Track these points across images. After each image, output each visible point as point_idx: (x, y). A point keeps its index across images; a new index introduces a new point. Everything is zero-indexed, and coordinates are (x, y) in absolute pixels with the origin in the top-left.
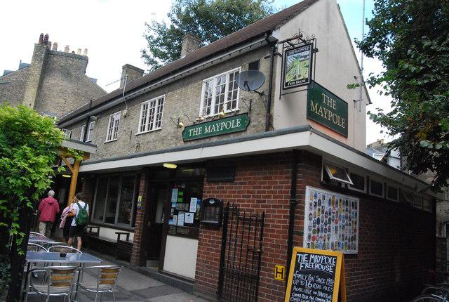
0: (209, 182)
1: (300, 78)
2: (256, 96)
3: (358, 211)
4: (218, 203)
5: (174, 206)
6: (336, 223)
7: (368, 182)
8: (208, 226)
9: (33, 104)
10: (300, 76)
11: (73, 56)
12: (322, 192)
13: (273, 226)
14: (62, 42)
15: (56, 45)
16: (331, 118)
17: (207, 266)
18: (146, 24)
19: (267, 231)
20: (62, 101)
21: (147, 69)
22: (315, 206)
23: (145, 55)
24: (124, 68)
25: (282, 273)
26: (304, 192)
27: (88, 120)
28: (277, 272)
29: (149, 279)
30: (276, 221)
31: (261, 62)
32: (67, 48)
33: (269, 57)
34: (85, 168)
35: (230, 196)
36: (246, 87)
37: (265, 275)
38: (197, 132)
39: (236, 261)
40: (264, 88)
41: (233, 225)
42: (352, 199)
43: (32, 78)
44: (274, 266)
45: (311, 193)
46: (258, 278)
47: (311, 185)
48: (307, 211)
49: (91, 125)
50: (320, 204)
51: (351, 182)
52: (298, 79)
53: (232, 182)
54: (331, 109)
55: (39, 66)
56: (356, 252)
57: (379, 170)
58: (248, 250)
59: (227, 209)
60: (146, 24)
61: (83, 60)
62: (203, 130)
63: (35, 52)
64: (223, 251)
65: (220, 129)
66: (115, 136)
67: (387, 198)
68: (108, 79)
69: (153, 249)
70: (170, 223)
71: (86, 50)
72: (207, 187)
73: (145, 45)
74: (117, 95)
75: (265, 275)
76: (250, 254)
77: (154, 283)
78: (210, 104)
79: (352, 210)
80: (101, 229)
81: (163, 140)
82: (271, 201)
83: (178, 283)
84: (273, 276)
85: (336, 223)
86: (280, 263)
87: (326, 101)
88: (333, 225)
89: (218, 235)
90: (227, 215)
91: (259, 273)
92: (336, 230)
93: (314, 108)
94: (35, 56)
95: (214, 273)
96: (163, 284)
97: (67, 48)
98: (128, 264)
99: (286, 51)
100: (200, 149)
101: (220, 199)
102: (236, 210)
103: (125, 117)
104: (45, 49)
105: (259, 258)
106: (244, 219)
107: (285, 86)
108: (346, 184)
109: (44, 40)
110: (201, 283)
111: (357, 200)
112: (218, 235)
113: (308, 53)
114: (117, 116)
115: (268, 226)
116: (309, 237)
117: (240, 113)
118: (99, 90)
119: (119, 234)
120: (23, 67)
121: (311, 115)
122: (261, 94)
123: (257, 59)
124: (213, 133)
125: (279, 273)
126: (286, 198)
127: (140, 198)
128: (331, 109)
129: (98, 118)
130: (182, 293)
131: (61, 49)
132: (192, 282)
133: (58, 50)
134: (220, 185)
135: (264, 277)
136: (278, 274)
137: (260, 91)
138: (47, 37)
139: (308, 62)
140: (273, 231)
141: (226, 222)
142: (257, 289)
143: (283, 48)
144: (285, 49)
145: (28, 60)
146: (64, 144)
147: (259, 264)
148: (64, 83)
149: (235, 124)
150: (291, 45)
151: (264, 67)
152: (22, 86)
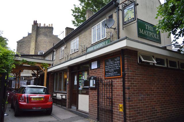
1: (130, 19)
2: (113, 30)
7: (179, 64)
10: (130, 18)
11: (47, 28)
13: (117, 86)
14: (43, 22)
15: (40, 24)
16: (151, 35)
17: (93, 107)
18: (72, 10)
19: (114, 88)
20: (45, 46)
21: (75, 28)
23: (74, 22)
24: (66, 29)
25: (122, 108)
27: (54, 51)
28: (120, 108)
29: (71, 113)
32: (45, 25)
33: (116, 12)
34: (49, 70)
35: (99, 75)
36: (106, 26)
37: (115, 109)
39: (104, 104)
40: (115, 26)
43: (32, 38)
44: (118, 105)
46: (112, 111)
49: (55, 53)
51: (155, 62)
52: (130, 19)
54: (151, 31)
55: (35, 33)
57: (177, 56)
58: (107, 98)
60: (72, 10)
63: (32, 28)
64: (98, 100)
66: (63, 56)
67: (169, 67)
68: (60, 33)
69: (74, 101)
70: (79, 89)
71: (52, 24)
73: (73, 19)
74: (65, 39)
75: (115, 109)
77: (75, 115)
80: (57, 94)
83: (82, 115)
84: (118, 110)
86: (121, 103)
89: (95, 92)
90: (98, 83)
91: (112, 109)
93: (141, 31)
94: (33, 30)
95: (96, 110)
96: (77, 116)
97: (45, 25)
98: (65, 107)
99: (123, 8)
100: (85, 56)
101: (95, 76)
103: (66, 48)
104: (36, 26)
106: (104, 84)
107: (124, 23)
108: (154, 64)
109: (35, 23)
110: (91, 114)
112: (95, 92)
113: (133, 6)
114: (63, 48)
115: (115, 86)
118: (59, 39)
119: (62, 95)
120: (29, 34)
121: (140, 35)
122: (115, 29)
123: (112, 14)
125: (121, 108)
128: (151, 31)
129: (56, 50)
130: (80, 119)
131: (42, 25)
132: (88, 114)
133: (41, 26)
136: (121, 107)
137: (114, 28)
138: (36, 21)
139: (133, 11)
140: (117, 88)
143: (122, 6)
144: (123, 7)
145: (30, 32)
147: (112, 104)
148: (45, 38)
150: (126, 4)
152: (30, 42)
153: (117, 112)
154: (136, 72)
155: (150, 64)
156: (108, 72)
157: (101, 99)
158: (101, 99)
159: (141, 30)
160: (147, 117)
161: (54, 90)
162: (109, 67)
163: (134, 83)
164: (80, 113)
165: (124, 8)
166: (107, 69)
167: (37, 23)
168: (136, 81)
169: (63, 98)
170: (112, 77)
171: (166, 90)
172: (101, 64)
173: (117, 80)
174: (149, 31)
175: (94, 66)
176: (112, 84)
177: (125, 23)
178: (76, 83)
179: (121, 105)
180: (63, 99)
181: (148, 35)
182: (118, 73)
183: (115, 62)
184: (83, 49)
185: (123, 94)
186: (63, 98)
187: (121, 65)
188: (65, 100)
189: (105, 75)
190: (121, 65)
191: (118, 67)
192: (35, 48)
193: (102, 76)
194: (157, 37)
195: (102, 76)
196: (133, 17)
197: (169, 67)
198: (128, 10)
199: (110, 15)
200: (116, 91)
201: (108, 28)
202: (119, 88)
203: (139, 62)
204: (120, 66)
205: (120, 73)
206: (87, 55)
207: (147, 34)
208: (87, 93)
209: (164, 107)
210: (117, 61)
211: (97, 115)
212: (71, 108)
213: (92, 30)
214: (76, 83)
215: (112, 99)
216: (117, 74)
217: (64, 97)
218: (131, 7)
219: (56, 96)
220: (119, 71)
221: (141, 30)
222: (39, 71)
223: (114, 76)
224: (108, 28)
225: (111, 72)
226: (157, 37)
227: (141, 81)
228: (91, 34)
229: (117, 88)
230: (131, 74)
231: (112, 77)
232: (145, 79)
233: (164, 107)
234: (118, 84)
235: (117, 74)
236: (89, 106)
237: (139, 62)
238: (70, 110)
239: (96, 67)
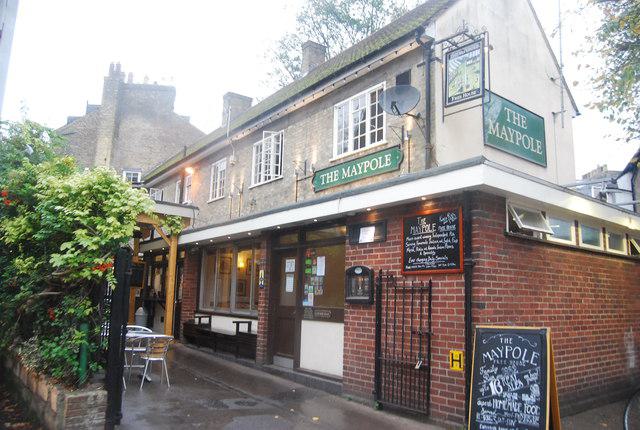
1: (469, 90)
8: (355, 304)
9: (109, 160)
10: (468, 87)
11: (156, 88)
14: (139, 73)
15: (131, 75)
16: (520, 142)
19: (437, 305)
24: (225, 98)
25: (460, 361)
32: (147, 78)
33: (424, 64)
34: (185, 240)
36: (395, 110)
38: (332, 177)
39: (394, 350)
41: (389, 299)
43: (104, 124)
44: (447, 352)
52: (465, 90)
61: (168, 93)
70: (305, 304)
80: (214, 318)
86: (458, 347)
89: (369, 315)
90: (380, 288)
97: (147, 78)
100: (337, 201)
107: (448, 102)
109: (115, 73)
112: (369, 315)
117: (389, 146)
119: (238, 323)
120: (91, 109)
123: (407, 69)
127: (262, 272)
131: (138, 80)
132: (340, 381)
133: (135, 82)
135: (437, 367)
138: (119, 66)
139: (478, 66)
140: (444, 305)
141: (380, 297)
148: (148, 126)
149: (383, 162)
150: (455, 44)
152: (92, 136)
153: (444, 372)
154: (500, 259)
155: (535, 236)
156: (416, 255)
157: (390, 337)
158: (390, 337)
161: (201, 304)
162: (420, 241)
163: (495, 292)
164: (317, 378)
165: (448, 56)
166: (411, 247)
167: (122, 70)
168: (500, 285)
169: (241, 330)
170: (427, 271)
171: (572, 312)
172: (389, 229)
173: (447, 281)
174: (515, 127)
175: (368, 235)
178: (290, 285)
179: (457, 353)
181: (512, 141)
182: (450, 261)
183: (442, 229)
186: (241, 330)
187: (461, 236)
189: (405, 262)
190: (461, 236)
191: (449, 244)
192: (112, 156)
193: (394, 267)
194: (535, 147)
195: (394, 267)
196: (478, 85)
198: (462, 61)
199: (402, 70)
200: (442, 311)
201: (399, 114)
202: (451, 305)
203: (508, 230)
204: (456, 241)
205: (457, 261)
206: (344, 200)
207: (509, 136)
208: (336, 317)
209: (564, 359)
210: (448, 223)
211: (372, 382)
212: (272, 363)
213: (336, 113)
214: (290, 285)
215: (429, 336)
216: (446, 262)
218: (471, 55)
219: (210, 324)
220: (452, 255)
222: (141, 240)
223: (438, 268)
224: (399, 114)
225: (427, 256)
226: (535, 147)
227: (512, 285)
228: (330, 127)
229: (444, 305)
230: (490, 264)
231: (427, 271)
232: (522, 280)
233: (564, 359)
234: (449, 291)
235: (446, 262)
236: (345, 356)
237: (508, 230)
238: (270, 369)
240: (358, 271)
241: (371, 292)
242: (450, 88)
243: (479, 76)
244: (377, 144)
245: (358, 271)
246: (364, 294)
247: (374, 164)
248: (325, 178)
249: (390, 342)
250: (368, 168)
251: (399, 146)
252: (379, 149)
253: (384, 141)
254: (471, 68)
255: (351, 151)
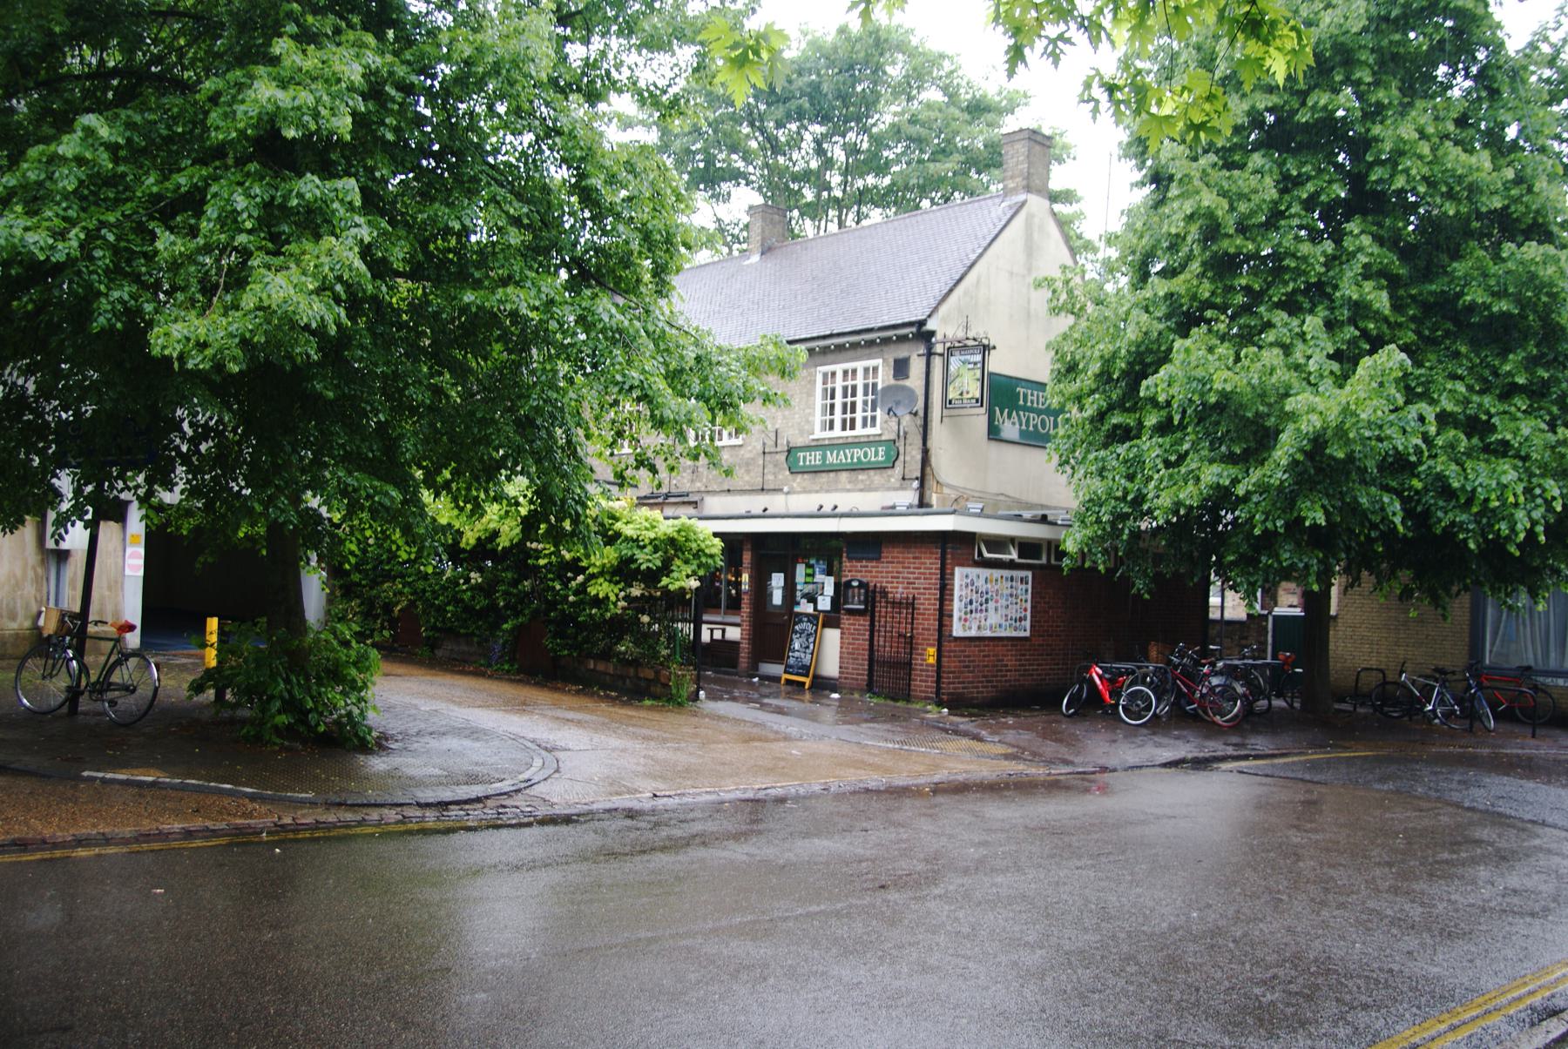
0: (850, 559)
3: (1030, 586)
4: (862, 585)
5: (799, 587)
6: (997, 601)
8: (851, 612)
12: (973, 572)
22: (967, 586)
26: (953, 574)
30: (928, 603)
31: (911, 361)
38: (814, 459)
39: (886, 649)
41: (881, 608)
42: (1018, 574)
45: (962, 574)
46: (911, 664)
47: (962, 565)
48: (957, 593)
50: (973, 584)
53: (878, 559)
54: (1083, 278)
56: (1027, 634)
59: (874, 592)
62: (824, 457)
65: (852, 458)
72: (847, 564)
76: (902, 640)
78: (833, 397)
79: (1020, 586)
81: (748, 464)
82: (920, 583)
85: (997, 601)
87: (1025, 400)
88: (991, 605)
89: (864, 622)
92: (996, 609)
101: (865, 580)
102: (884, 593)
105: (911, 643)
106: (893, 603)
107: (947, 403)
111: (1029, 574)
112: (864, 622)
116: (960, 619)
117: (883, 438)
124: (841, 464)
126: (935, 580)
134: (864, 563)
135: (917, 661)
141: (874, 607)
142: (910, 675)
146: (656, 514)
149: (876, 454)
151: (917, 366)
157: (882, 639)
158: (882, 639)
159: (1002, 414)
160: (984, 676)
176: (913, 604)
177: (950, 402)
179: (932, 651)
180: (717, 641)
184: (770, 443)
185: (1208, 591)
188: (734, 645)
197: (1053, 562)
217: (734, 634)
221: (1002, 414)
239: (958, 630)
240: (855, 584)
241: (866, 602)
242: (950, 388)
243: (979, 384)
244: (848, 433)
245: (855, 584)
246: (860, 603)
247: (866, 455)
248: (805, 458)
249: (881, 643)
250: (859, 458)
251: (894, 441)
252: (850, 440)
253: (877, 430)
254: (972, 373)
255: (837, 432)
